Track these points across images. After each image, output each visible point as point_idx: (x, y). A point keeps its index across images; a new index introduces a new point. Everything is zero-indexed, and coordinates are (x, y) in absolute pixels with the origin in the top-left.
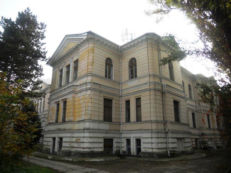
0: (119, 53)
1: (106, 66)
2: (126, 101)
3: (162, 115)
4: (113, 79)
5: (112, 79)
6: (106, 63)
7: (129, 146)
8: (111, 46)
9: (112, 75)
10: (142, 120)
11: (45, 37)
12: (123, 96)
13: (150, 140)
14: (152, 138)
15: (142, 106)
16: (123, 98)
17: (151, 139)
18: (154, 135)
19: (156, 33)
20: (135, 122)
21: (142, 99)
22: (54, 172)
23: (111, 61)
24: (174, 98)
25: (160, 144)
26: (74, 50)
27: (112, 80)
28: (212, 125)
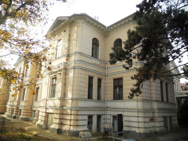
0: (106, 34)
1: (93, 46)
2: (115, 80)
3: (160, 96)
4: (99, 59)
5: (97, 58)
6: (93, 43)
7: (89, 120)
8: (101, 28)
9: (98, 55)
10: (123, 99)
11: (137, 11)
12: (109, 74)
13: (135, 119)
14: (138, 117)
15: (124, 86)
16: (109, 77)
17: (137, 118)
18: (141, 114)
19: (119, 20)
20: (112, 100)
21: (124, 79)
22: (38, 140)
23: (98, 42)
24: (52, 77)
25: (146, 124)
26: (114, 29)
27: (98, 59)
28: (70, 101)
